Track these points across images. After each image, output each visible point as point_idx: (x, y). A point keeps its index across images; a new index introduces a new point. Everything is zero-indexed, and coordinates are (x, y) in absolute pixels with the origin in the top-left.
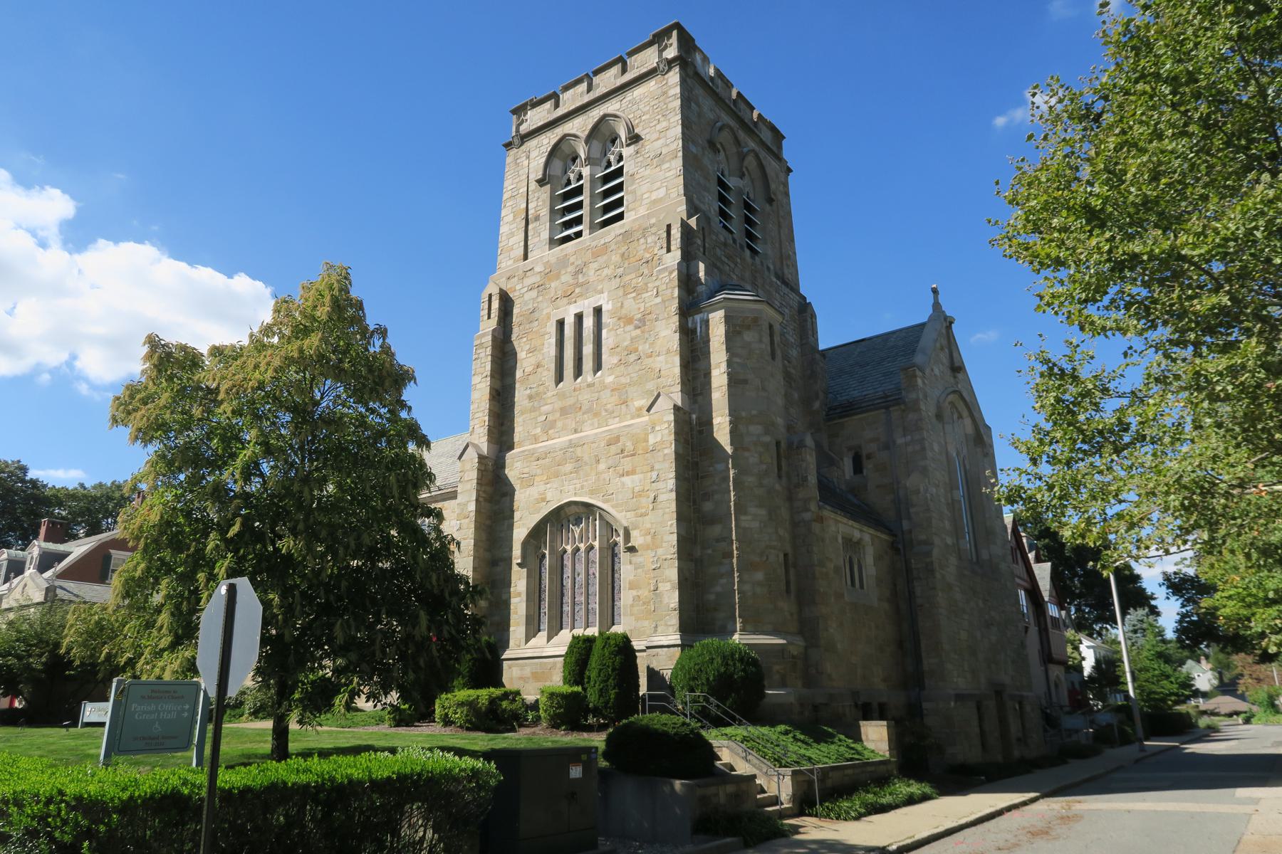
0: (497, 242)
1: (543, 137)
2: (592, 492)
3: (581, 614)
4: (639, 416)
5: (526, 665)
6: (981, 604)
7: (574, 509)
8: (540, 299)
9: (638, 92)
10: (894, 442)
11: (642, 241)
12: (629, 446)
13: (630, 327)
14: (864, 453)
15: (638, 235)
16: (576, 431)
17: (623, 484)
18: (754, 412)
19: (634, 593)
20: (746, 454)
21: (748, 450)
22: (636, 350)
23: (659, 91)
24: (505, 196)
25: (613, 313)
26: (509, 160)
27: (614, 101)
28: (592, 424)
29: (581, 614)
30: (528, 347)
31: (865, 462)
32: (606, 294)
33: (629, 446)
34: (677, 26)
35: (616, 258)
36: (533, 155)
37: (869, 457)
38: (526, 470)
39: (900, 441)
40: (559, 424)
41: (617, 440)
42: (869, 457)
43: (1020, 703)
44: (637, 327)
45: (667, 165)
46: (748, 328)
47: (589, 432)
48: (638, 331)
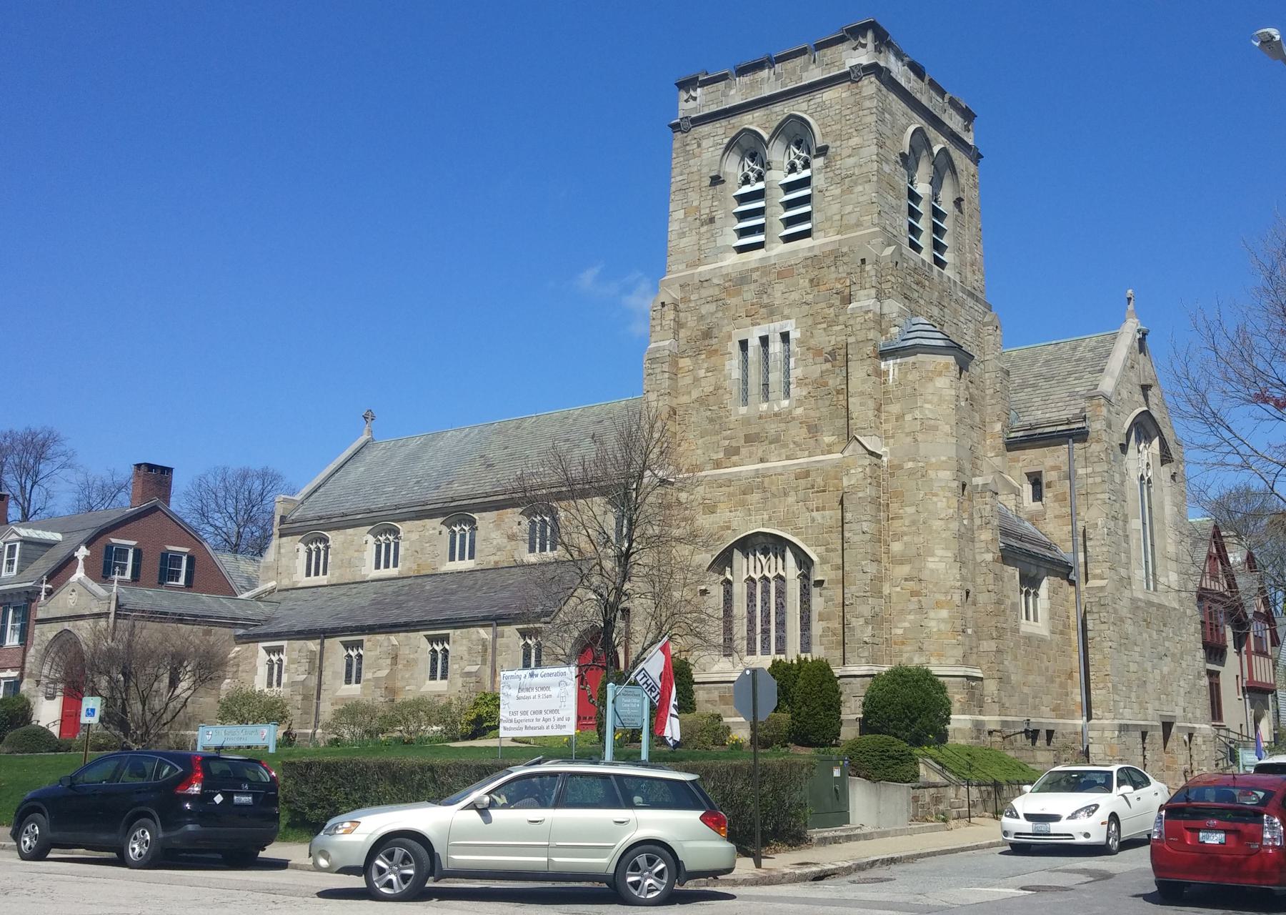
0: (666, 241)
1: (717, 124)
2: (780, 525)
3: (765, 641)
4: (830, 452)
5: (710, 689)
6: (1155, 636)
7: (761, 539)
8: (720, 314)
9: (829, 95)
10: (1076, 472)
11: (833, 269)
12: (820, 481)
13: (821, 359)
14: (1044, 481)
15: (829, 261)
16: (762, 461)
17: (813, 520)
18: (943, 458)
19: (824, 624)
20: (935, 499)
21: (936, 495)
22: (826, 384)
23: (852, 100)
24: (673, 188)
25: (800, 342)
26: (676, 145)
27: (800, 99)
28: (780, 455)
29: (765, 641)
30: (706, 365)
31: (1044, 490)
32: (793, 321)
33: (820, 481)
34: (873, 26)
35: (804, 283)
36: (705, 143)
37: (1049, 485)
38: (708, 496)
39: (1081, 471)
40: (743, 451)
41: (806, 474)
42: (1049, 485)
43: (1190, 736)
44: (826, 361)
45: (860, 188)
46: (940, 374)
47: (774, 464)
48: (828, 365)
